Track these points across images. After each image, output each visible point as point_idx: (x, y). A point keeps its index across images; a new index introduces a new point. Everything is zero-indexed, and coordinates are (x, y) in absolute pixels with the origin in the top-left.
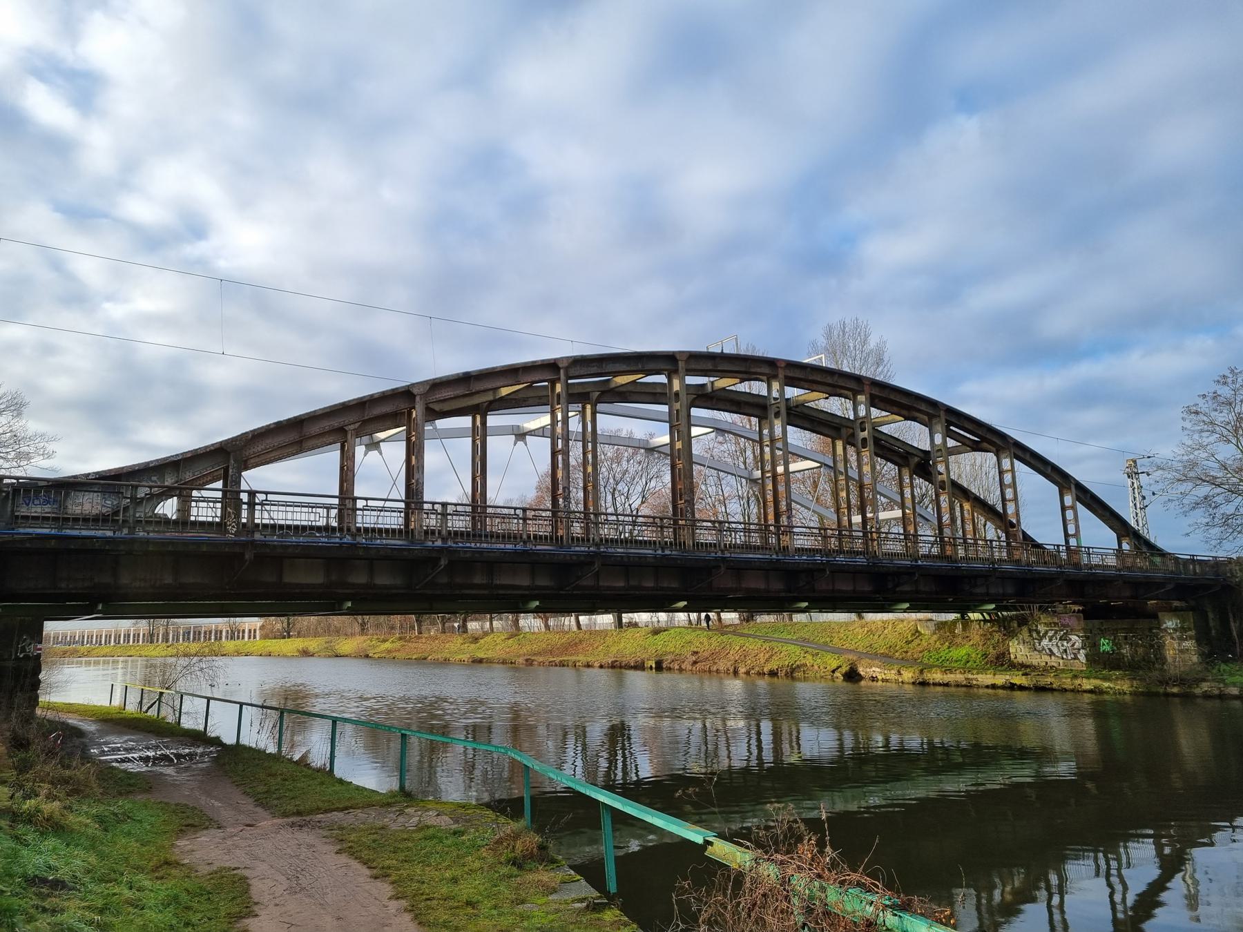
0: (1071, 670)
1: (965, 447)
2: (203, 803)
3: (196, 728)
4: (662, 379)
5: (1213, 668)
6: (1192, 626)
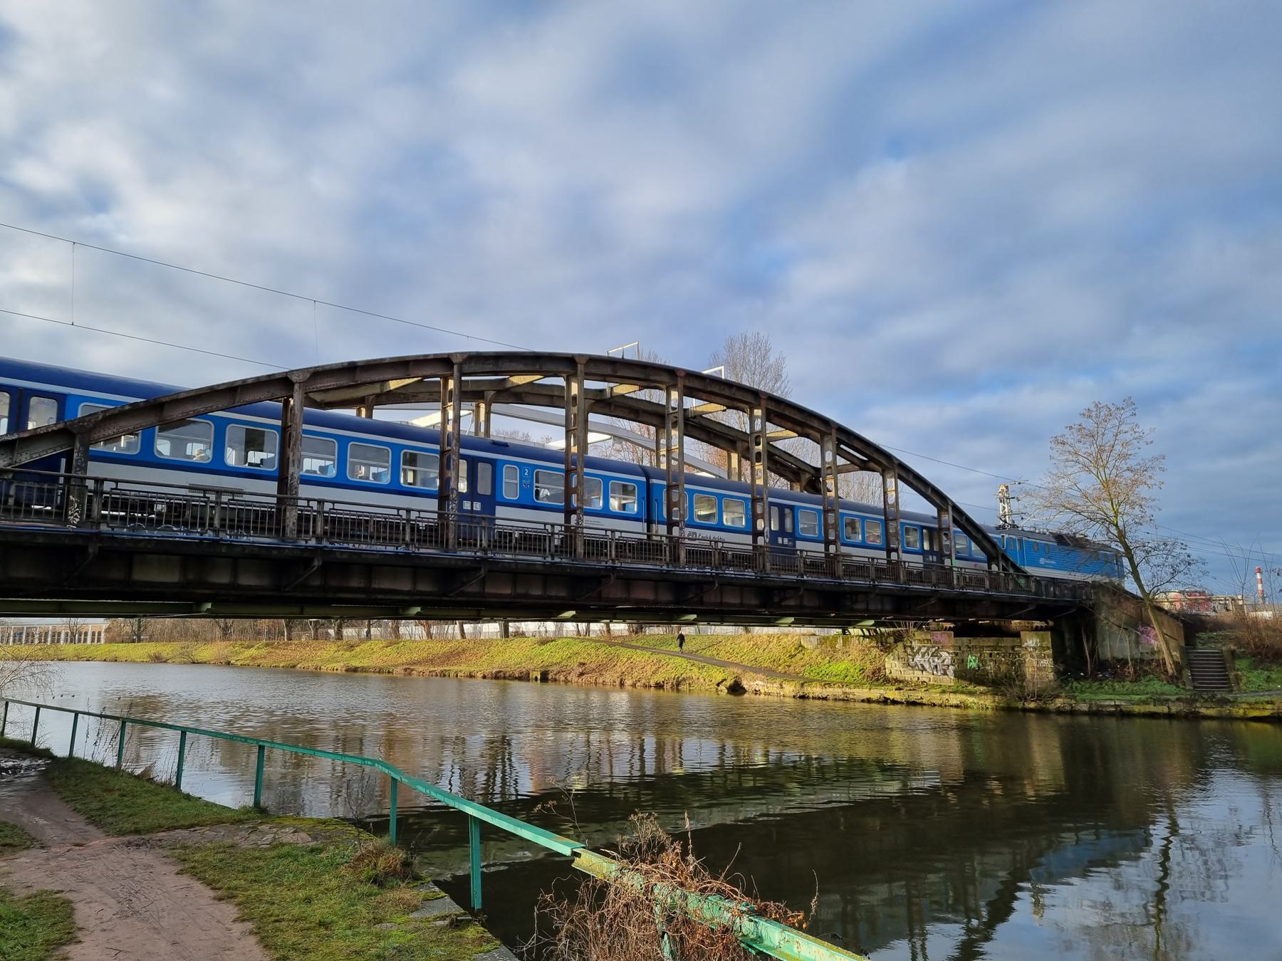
0: (941, 686)
1: (853, 466)
2: (25, 820)
3: (23, 738)
4: (560, 381)
5: (1067, 686)
6: (1050, 645)
